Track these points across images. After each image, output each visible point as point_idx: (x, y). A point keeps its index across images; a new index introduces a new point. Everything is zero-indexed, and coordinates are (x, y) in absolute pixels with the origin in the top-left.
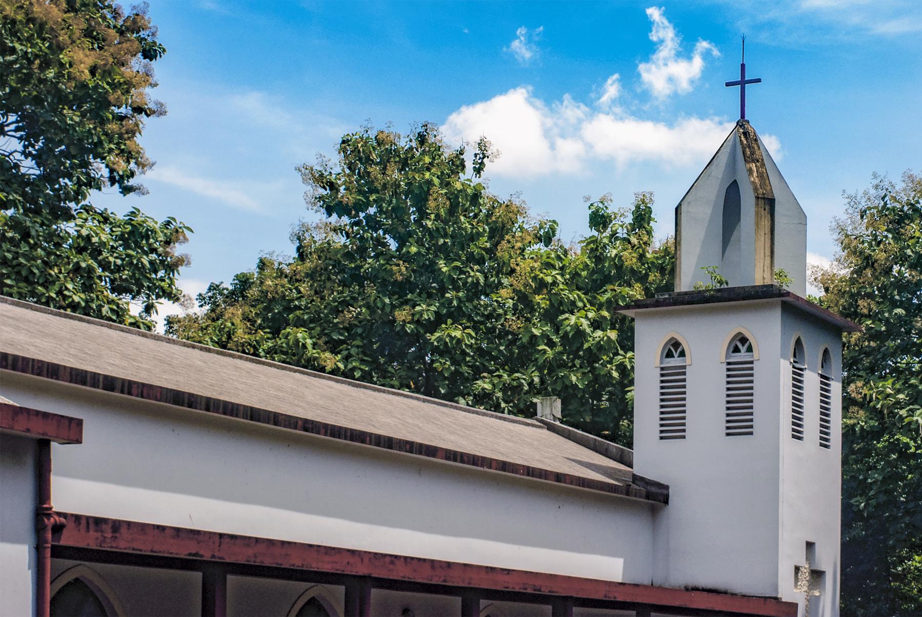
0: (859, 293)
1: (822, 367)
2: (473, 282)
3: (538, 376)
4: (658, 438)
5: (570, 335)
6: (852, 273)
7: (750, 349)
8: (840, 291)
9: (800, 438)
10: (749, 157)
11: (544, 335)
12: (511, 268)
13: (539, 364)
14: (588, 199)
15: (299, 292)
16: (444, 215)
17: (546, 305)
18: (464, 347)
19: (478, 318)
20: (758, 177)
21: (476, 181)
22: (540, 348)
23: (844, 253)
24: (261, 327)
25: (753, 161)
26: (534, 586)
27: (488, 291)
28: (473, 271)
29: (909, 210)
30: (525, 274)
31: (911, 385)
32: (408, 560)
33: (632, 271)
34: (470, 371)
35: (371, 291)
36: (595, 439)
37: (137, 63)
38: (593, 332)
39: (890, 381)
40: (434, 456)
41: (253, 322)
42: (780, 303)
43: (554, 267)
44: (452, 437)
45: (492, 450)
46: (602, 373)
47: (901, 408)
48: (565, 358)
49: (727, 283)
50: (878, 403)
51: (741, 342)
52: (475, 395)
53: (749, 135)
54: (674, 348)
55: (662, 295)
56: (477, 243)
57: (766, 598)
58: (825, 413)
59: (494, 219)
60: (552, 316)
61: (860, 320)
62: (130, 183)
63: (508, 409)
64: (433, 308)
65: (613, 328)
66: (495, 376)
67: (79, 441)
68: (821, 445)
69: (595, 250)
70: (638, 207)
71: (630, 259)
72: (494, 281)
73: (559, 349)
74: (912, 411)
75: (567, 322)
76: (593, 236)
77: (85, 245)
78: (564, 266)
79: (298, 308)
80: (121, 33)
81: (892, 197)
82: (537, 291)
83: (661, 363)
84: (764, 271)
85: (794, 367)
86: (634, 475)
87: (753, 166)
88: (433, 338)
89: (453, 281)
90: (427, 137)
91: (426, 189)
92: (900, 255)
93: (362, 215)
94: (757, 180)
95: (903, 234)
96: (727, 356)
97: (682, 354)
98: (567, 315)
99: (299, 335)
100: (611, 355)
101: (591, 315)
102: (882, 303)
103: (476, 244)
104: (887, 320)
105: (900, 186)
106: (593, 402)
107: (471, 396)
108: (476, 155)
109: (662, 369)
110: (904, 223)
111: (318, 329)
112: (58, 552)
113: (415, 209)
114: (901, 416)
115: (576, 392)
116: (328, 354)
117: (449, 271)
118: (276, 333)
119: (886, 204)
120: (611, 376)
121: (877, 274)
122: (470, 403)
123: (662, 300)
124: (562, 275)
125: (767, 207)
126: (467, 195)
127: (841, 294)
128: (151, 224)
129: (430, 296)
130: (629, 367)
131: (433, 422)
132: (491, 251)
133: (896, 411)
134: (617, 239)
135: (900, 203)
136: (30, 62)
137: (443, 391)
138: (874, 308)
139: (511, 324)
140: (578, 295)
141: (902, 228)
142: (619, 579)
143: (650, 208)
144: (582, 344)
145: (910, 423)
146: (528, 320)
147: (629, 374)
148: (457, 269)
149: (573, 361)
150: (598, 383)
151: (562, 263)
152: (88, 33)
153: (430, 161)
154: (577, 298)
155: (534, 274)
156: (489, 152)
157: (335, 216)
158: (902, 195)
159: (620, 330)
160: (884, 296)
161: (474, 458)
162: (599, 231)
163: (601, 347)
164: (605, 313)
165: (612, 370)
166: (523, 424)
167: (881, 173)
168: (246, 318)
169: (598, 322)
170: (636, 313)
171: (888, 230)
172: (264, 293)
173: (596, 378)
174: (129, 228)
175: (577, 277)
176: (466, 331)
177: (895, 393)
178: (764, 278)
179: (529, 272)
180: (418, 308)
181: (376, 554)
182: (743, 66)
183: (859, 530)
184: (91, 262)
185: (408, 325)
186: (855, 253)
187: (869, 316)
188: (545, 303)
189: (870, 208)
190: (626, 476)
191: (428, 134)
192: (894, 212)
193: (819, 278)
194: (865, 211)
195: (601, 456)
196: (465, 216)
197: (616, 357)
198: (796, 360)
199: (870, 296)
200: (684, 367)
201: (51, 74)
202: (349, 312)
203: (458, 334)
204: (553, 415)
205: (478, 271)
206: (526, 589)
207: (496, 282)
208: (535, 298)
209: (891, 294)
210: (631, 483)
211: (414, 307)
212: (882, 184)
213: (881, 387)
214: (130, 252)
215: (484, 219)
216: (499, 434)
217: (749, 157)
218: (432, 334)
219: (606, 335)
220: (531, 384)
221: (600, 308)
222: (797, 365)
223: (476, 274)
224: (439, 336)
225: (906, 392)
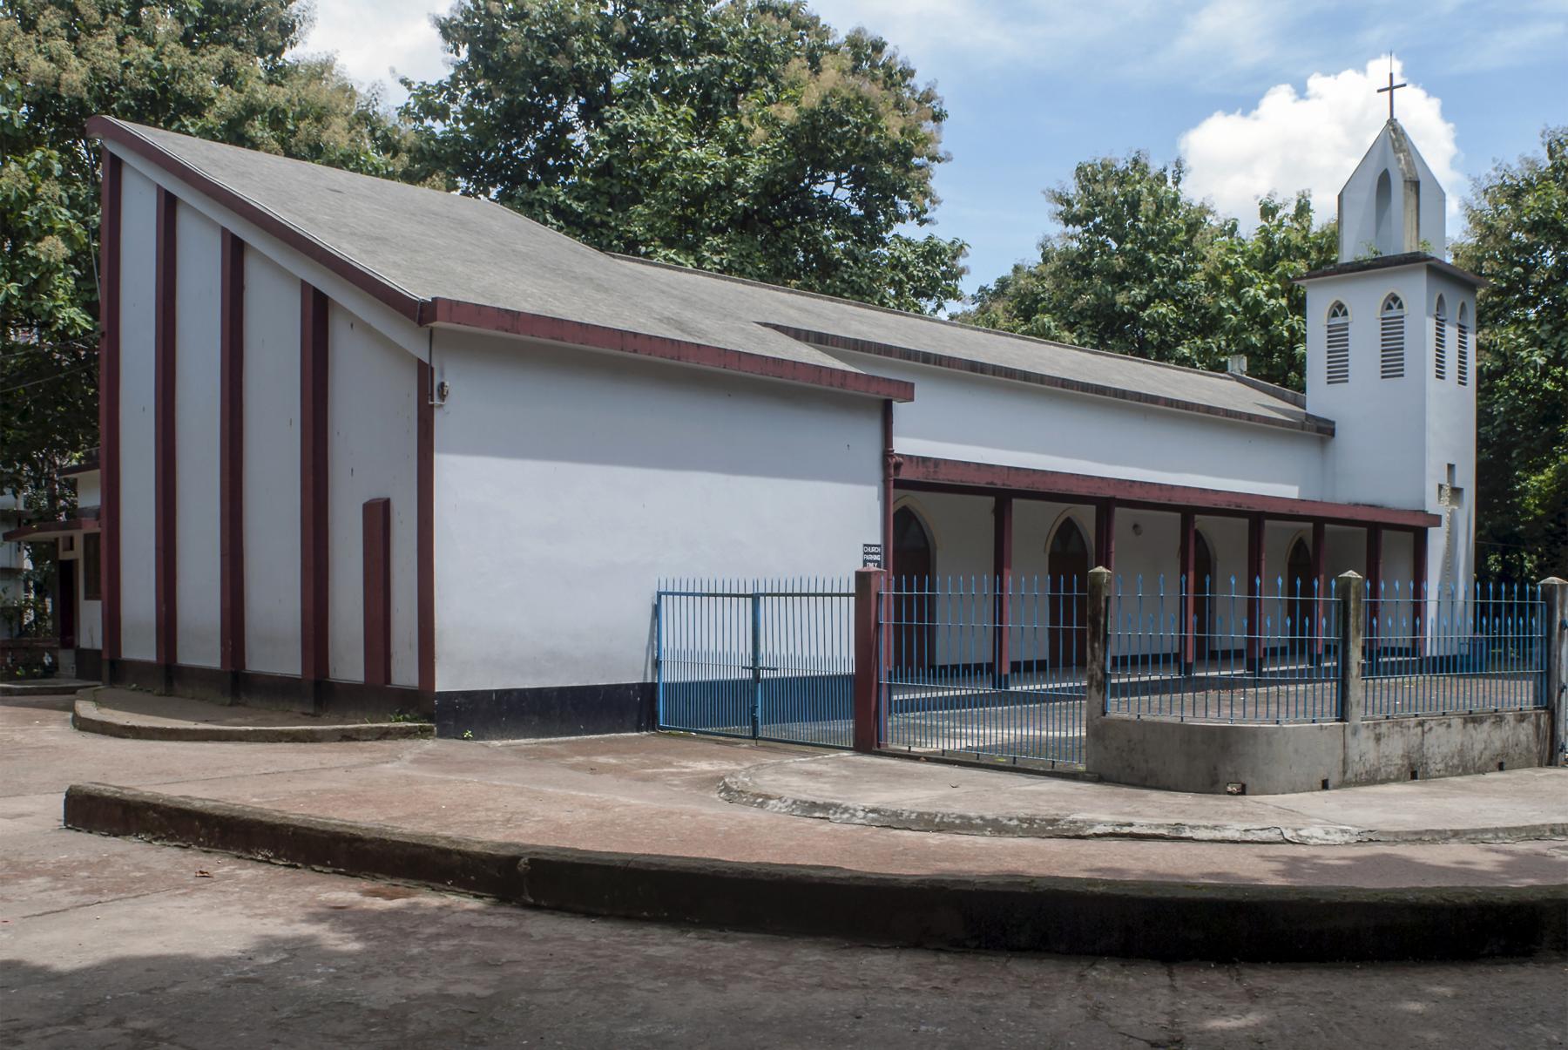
0: (1483, 256)
6: (1478, 241)
7: (1401, 306)
9: (1442, 378)
15: (1044, 287)
24: (1016, 316)
31: (1532, 331)
33: (1298, 248)
35: (1098, 281)
37: (928, 126)
39: (1513, 328)
41: (1011, 313)
43: (1236, 252)
51: (1393, 301)
54: (1339, 309)
58: (1462, 355)
60: (1235, 291)
62: (925, 216)
65: (1283, 297)
67: (912, 399)
68: (1460, 383)
69: (1266, 235)
70: (1299, 201)
71: (1296, 238)
73: (1240, 317)
74: (1532, 352)
75: (1247, 295)
77: (897, 264)
79: (1043, 299)
80: (919, 102)
82: (1224, 272)
86: (1307, 414)
87: (1401, 155)
89: (1160, 269)
93: (1091, 224)
94: (1405, 168)
96: (1382, 313)
97: (1345, 313)
99: (1046, 320)
101: (1266, 287)
104: (1508, 278)
105: (1516, 166)
109: (1329, 326)
111: (1059, 314)
112: (900, 484)
116: (1066, 333)
118: (1027, 319)
119: (1504, 182)
124: (1242, 258)
125: (1414, 189)
127: (1470, 258)
128: (942, 244)
132: (1188, 243)
136: (859, 130)
145: (1529, 363)
149: (1252, 326)
150: (1273, 342)
152: (897, 106)
157: (1070, 226)
159: (1289, 299)
160: (1505, 258)
162: (1267, 221)
163: (1273, 313)
164: (1278, 286)
168: (1006, 310)
172: (1018, 290)
173: (1272, 337)
174: (928, 248)
180: (1133, 292)
183: (1486, 455)
184: (901, 275)
187: (1491, 276)
189: (1491, 187)
199: (1493, 258)
200: (1347, 324)
201: (873, 137)
202: (1082, 299)
203: (1163, 310)
214: (929, 268)
220: (1219, 347)
221: (1272, 281)
222: (1440, 318)
223: (1177, 261)
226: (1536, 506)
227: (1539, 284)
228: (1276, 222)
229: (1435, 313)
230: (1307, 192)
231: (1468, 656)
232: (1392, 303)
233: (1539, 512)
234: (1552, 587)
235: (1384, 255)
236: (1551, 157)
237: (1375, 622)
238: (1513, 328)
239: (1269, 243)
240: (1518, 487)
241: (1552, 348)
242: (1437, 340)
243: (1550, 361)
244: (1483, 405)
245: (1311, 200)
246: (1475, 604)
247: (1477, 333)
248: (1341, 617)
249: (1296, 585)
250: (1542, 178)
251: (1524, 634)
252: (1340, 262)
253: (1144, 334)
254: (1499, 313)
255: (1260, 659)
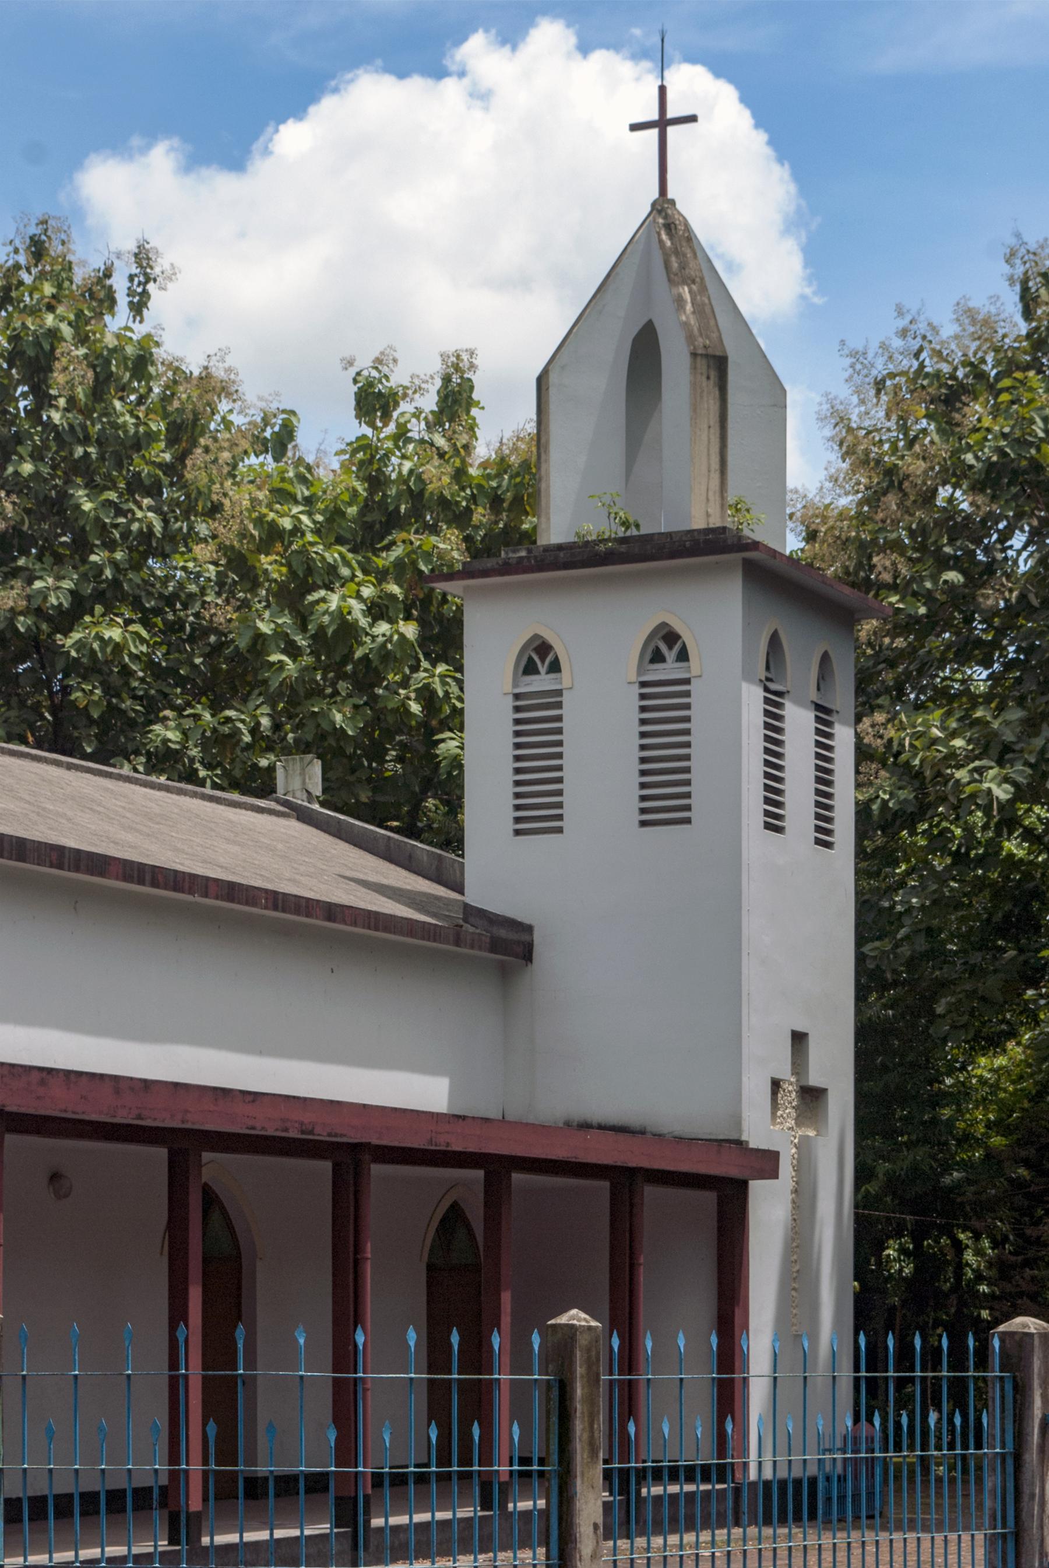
0: (874, 541)
1: (819, 689)
2: (141, 530)
3: (268, 714)
4: (511, 832)
5: (330, 631)
6: (860, 503)
7: (683, 656)
8: (838, 538)
9: (779, 830)
10: (676, 275)
11: (280, 634)
12: (212, 502)
13: (272, 689)
14: (351, 363)
16: (83, 400)
17: (281, 575)
18: (127, 659)
19: (153, 603)
20: (694, 313)
21: (139, 330)
22: (274, 658)
23: (844, 465)
25: (684, 282)
26: (302, 1123)
27: (168, 549)
28: (140, 508)
29: (966, 376)
30: (241, 513)
31: (978, 721)
32: (72, 1077)
33: (444, 503)
34: (138, 708)
36: (389, 837)
38: (371, 626)
39: (938, 713)
40: (102, 874)
42: (741, 562)
44: (130, 837)
45: (204, 861)
46: (391, 705)
47: (959, 767)
48: (319, 678)
49: (637, 526)
50: (916, 755)
52: (149, 754)
53: (676, 228)
55: (514, 552)
56: (147, 455)
57: (720, 1142)
58: (824, 777)
59: (176, 404)
61: (876, 595)
63: (213, 782)
64: (67, 584)
65: (408, 618)
66: (188, 716)
70: (447, 379)
72: (181, 528)
73: (307, 660)
74: (979, 770)
75: (322, 607)
76: (364, 436)
78: (313, 495)
81: (933, 350)
82: (265, 546)
83: (515, 684)
84: (708, 500)
85: (766, 689)
86: (466, 907)
88: (69, 642)
90: (47, 245)
91: (47, 347)
92: (953, 464)
94: (693, 321)
95: (958, 425)
96: (640, 670)
97: (555, 667)
98: (322, 593)
100: (407, 671)
101: (367, 592)
102: (918, 560)
103: (144, 456)
105: (948, 330)
106: (370, 765)
107: (141, 755)
108: (131, 278)
109: (517, 697)
110: (961, 401)
113: (26, 389)
114: (958, 781)
115: (342, 744)
117: (95, 509)
119: (922, 366)
120: (407, 711)
121: (908, 503)
122: (141, 768)
123: (514, 561)
124: (310, 514)
126: (126, 358)
129: (59, 560)
130: (441, 694)
131: (91, 809)
133: (949, 771)
134: (409, 440)
135: (948, 362)
137: (89, 750)
138: (904, 571)
139: (215, 614)
140: (340, 554)
141: (958, 410)
142: (445, 1112)
143: (470, 380)
144: (352, 652)
145: (973, 796)
146: (245, 604)
147: (441, 707)
148: (110, 506)
149: (333, 684)
151: (308, 489)
153: (54, 291)
154: (339, 559)
155: (257, 514)
156: (157, 270)
158: (953, 346)
159: (422, 623)
160: (922, 548)
161: (176, 877)
162: (372, 424)
163: (385, 656)
164: (395, 589)
165: (409, 699)
166: (252, 810)
167: (912, 305)
169: (379, 607)
170: (466, 589)
171: (928, 416)
175: (338, 520)
176: (130, 628)
177: (946, 737)
178: (708, 515)
179: (247, 509)
180: (38, 584)
181: (13, 1066)
182: (662, 90)
185: (22, 618)
186: (865, 462)
187: (894, 588)
188: (279, 571)
189: (892, 375)
190: (450, 908)
191: (49, 237)
192: (938, 381)
193: (799, 514)
194: (883, 381)
195: (399, 869)
196: (121, 399)
197: (415, 675)
198: (769, 676)
199: (896, 546)
200: (559, 693)
203: (115, 634)
204: (307, 791)
205: (150, 509)
206: (286, 1130)
207: (185, 530)
208: (259, 561)
209: (936, 541)
210: (461, 922)
211: (30, 582)
212: (914, 327)
213: (920, 725)
215: (158, 405)
216: (212, 830)
217: (676, 275)
218: (66, 635)
219: (397, 631)
220: (255, 730)
222: (773, 686)
224: (80, 639)
225: (968, 734)
226: (989, 1125)
227: (996, 613)
228: (391, 428)
229: (762, 674)
230: (465, 357)
231: (842, 1479)
232: (664, 648)
233: (997, 1141)
234: (1024, 1339)
235: (644, 531)
236: (1028, 314)
237: (632, 1429)
238: (938, 713)
239: (376, 481)
240: (948, 1081)
241: (1026, 763)
242: (767, 738)
243: (1020, 794)
244: (874, 891)
245: (476, 378)
246: (857, 1380)
247: (858, 719)
248: (555, 1419)
249: (450, 1345)
250: (1010, 365)
251: (965, 1447)
252: (543, 541)
253: (66, 690)
254: (907, 673)
255: (366, 1497)
